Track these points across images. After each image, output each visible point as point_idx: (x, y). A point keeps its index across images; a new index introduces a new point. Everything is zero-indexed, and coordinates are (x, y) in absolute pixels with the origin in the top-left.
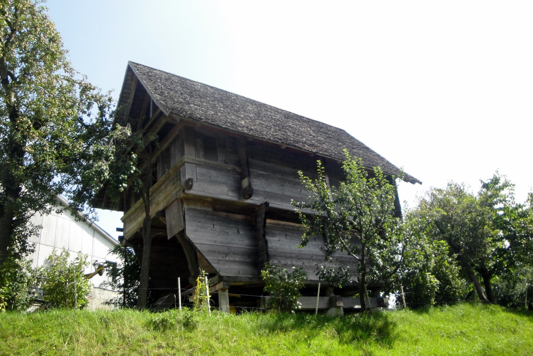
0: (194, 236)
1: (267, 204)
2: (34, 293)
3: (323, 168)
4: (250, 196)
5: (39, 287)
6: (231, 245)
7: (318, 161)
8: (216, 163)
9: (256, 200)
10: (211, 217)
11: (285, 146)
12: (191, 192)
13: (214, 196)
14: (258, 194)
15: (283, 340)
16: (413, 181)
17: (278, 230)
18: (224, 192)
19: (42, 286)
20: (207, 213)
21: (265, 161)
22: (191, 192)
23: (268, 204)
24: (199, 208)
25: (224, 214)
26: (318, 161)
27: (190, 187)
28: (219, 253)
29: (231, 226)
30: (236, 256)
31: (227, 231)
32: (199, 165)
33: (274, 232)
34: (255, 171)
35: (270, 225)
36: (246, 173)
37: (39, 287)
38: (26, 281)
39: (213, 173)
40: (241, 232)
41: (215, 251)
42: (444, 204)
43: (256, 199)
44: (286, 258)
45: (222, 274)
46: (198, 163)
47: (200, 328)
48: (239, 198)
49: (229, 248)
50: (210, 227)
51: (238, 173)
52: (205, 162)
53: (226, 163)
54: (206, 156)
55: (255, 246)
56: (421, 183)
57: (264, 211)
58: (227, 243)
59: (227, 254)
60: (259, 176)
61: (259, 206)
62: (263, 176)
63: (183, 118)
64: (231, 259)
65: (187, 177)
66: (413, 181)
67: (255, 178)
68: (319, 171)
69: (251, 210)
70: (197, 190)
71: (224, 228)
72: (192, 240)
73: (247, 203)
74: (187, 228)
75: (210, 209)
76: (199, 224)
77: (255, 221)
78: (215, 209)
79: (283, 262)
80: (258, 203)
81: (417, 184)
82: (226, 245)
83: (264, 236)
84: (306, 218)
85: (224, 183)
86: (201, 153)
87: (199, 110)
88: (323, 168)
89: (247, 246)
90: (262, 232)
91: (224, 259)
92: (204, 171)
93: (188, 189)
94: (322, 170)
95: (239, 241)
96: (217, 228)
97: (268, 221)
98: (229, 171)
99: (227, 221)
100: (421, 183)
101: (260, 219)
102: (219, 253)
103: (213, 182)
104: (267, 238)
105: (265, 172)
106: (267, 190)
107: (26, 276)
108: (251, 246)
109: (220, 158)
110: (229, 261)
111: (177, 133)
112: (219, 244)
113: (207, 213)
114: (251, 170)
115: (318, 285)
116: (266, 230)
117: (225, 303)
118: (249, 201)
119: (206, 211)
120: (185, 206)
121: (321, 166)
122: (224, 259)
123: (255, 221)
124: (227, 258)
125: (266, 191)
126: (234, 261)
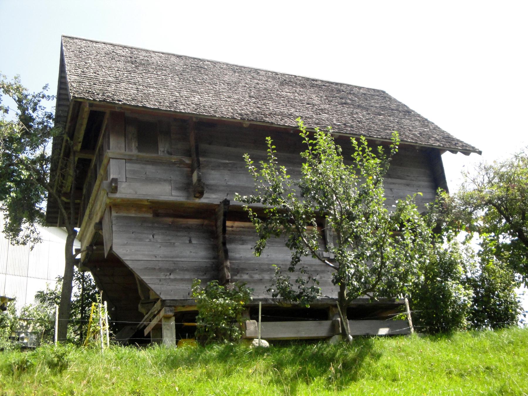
0: (125, 252)
1: (226, 202)
2: (23, 339)
3: (274, 147)
4: (201, 194)
5: (29, 331)
6: (178, 259)
7: (267, 138)
8: (154, 155)
9: (211, 198)
10: (150, 225)
11: (248, 123)
12: (117, 195)
13: (156, 198)
14: (213, 189)
15: (184, 377)
16: (467, 150)
17: (251, 235)
18: (166, 192)
19: (34, 329)
20: (144, 220)
21: (228, 146)
22: (117, 195)
23: (229, 201)
24: (133, 215)
25: (169, 220)
26: (267, 138)
27: (115, 190)
28: (160, 270)
29: (179, 234)
30: (186, 272)
31: (173, 241)
32: (129, 160)
33: (244, 237)
34: (213, 160)
35: (238, 229)
36: (196, 165)
37: (29, 331)
38: (9, 325)
39: (150, 169)
40: (194, 242)
41: (155, 269)
42: (507, 179)
43: (214, 196)
44: (262, 271)
45: (163, 297)
46: (127, 158)
47: (72, 369)
48: (188, 197)
49: (174, 263)
50: (148, 238)
51: (188, 166)
52: (138, 156)
53: (170, 154)
54: (140, 148)
55: (214, 258)
56: (480, 153)
57: (221, 212)
58: (173, 257)
59: (171, 271)
60: (218, 167)
61: (218, 205)
62: (225, 166)
63: (93, 102)
64: (178, 277)
65: (112, 177)
66: (467, 150)
67: (212, 169)
68: (269, 152)
69: (207, 212)
70: (127, 191)
71: (169, 238)
72: (121, 256)
73: (199, 203)
74: (115, 241)
75: (150, 215)
76: (133, 235)
77: (215, 225)
78: (156, 215)
79: (257, 277)
80: (217, 202)
81: (472, 154)
82: (170, 259)
83: (224, 244)
84: (257, 217)
85: (165, 180)
86: (134, 145)
87: (127, 92)
88: (274, 147)
89: (203, 258)
90: (221, 240)
91: (167, 277)
92: (136, 167)
93: (112, 192)
94: (273, 149)
95: (193, 252)
96: (159, 238)
97: (228, 223)
98: (174, 164)
99: (175, 228)
100: (480, 153)
101: (220, 223)
102: (160, 270)
103: (149, 180)
104: (228, 246)
105: (229, 160)
106: (229, 183)
107: (8, 319)
108: (209, 258)
109: (161, 149)
110: (175, 280)
111: (106, 123)
112: (160, 259)
113: (144, 220)
114: (201, 159)
115: (259, 305)
116: (227, 236)
117: (169, 335)
118: (204, 200)
119: (143, 217)
120: (114, 214)
121: (272, 145)
122: (167, 277)
123: (215, 225)
124: (172, 277)
125: (223, 186)
126: (182, 280)
